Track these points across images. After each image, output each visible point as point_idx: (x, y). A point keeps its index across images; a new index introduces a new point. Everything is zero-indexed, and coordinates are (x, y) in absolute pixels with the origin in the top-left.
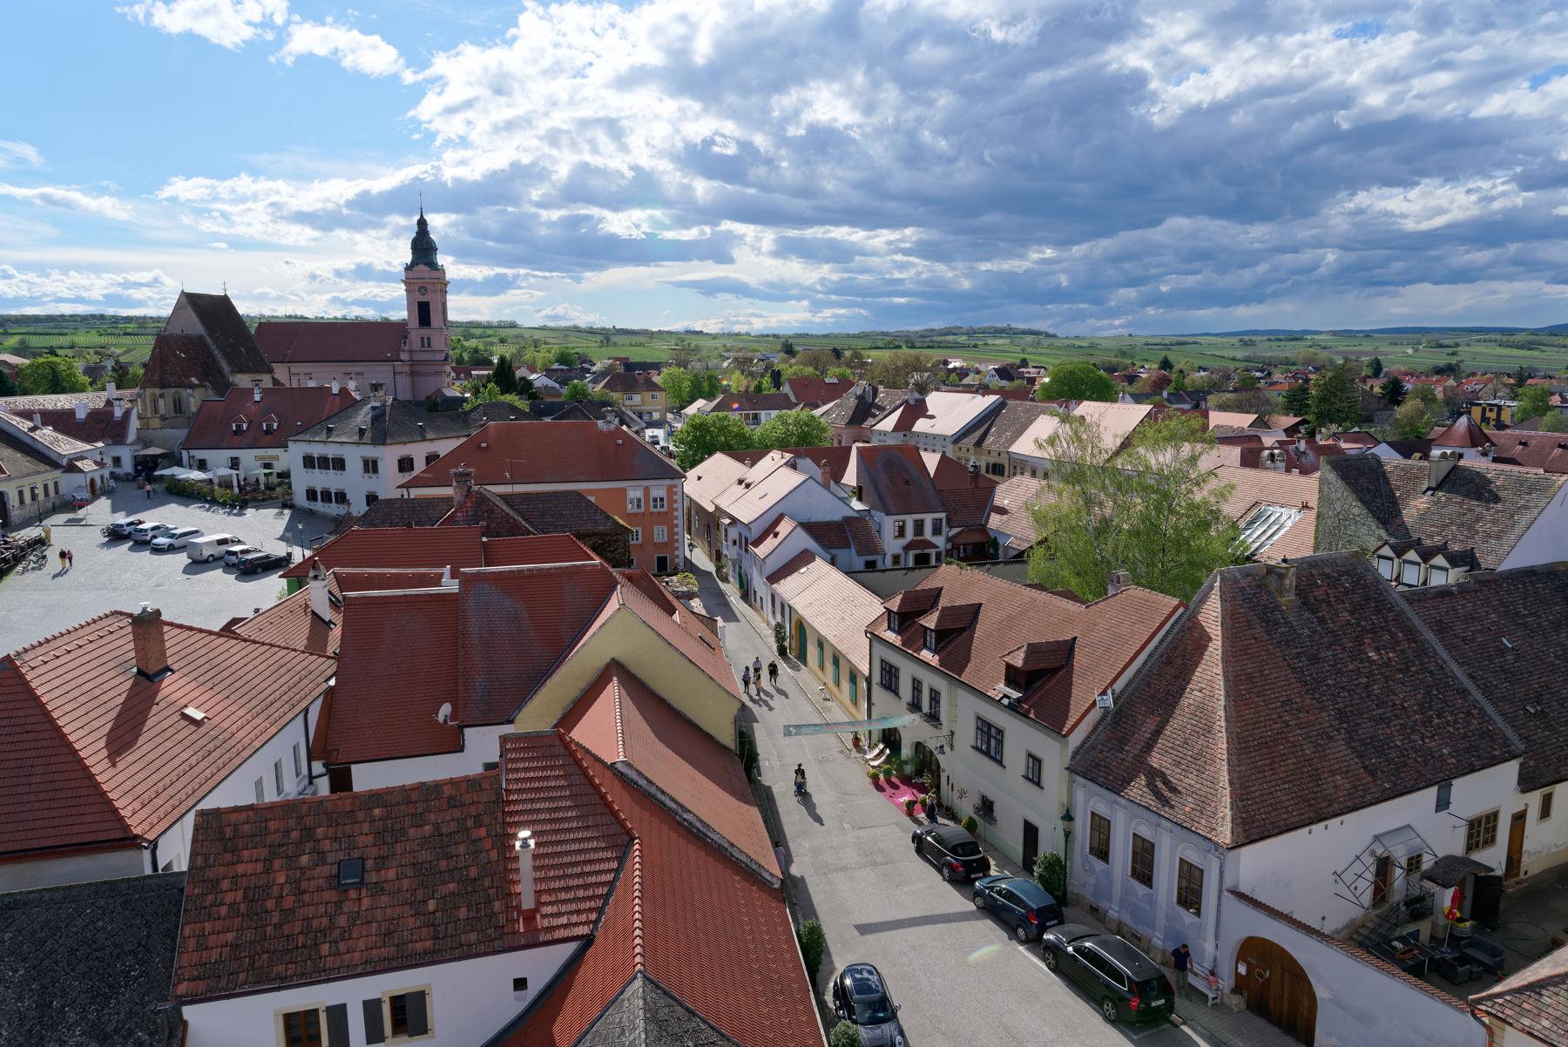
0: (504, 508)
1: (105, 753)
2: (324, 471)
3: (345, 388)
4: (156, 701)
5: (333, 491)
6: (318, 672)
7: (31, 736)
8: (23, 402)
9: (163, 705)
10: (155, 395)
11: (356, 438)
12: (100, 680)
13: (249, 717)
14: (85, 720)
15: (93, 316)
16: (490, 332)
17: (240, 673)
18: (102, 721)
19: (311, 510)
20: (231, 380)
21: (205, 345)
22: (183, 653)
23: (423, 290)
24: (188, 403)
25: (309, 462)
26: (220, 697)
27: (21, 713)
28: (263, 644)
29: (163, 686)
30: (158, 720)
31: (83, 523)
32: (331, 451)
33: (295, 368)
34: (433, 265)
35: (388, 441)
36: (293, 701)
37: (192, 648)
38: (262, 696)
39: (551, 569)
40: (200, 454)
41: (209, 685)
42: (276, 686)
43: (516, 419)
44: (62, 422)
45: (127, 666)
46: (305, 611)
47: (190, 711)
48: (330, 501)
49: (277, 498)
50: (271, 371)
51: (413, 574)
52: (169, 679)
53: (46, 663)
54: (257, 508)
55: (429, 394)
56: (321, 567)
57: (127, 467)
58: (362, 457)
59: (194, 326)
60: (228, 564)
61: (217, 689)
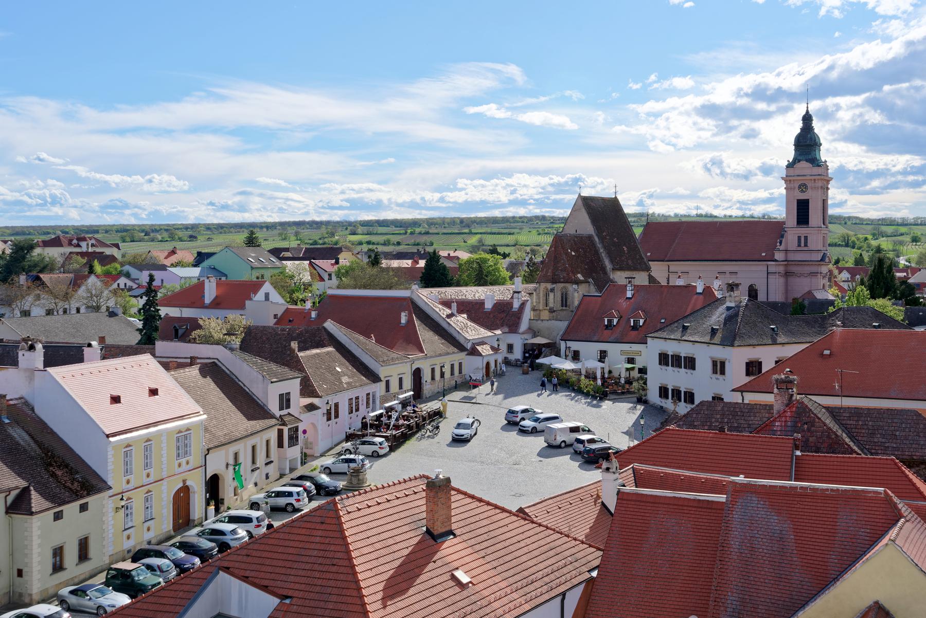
0: (828, 422)
1: (380, 595)
2: (676, 369)
3: (709, 287)
4: (433, 560)
5: (683, 390)
6: (584, 561)
7: (334, 569)
8: (450, 292)
9: (439, 563)
10: (547, 289)
11: (707, 339)
12: (395, 532)
13: (508, 590)
14: (375, 563)
15: (537, 217)
16: (903, 229)
17: (512, 548)
18: (387, 567)
19: (662, 407)
20: (611, 277)
21: (593, 244)
22: (468, 521)
23: (803, 187)
24: (573, 298)
25: (664, 359)
26: (489, 566)
27: (332, 548)
28: (540, 525)
29: (443, 547)
30: (431, 575)
31: (474, 401)
32: (684, 350)
33: (676, 266)
34: (815, 162)
35: (736, 343)
36: (553, 584)
37: (477, 518)
38: (526, 573)
39: (827, 490)
40: (575, 346)
41: (482, 553)
42: (541, 566)
43: (879, 327)
44: (473, 310)
45: (420, 524)
46: (595, 501)
47: (460, 574)
48: (667, 397)
49: (634, 393)
50: (648, 269)
51: (706, 479)
52: (450, 541)
53: (359, 510)
54: (614, 401)
55: (798, 295)
56: (614, 460)
57: (518, 354)
58: (711, 358)
59: (586, 227)
60: (576, 452)
61: (488, 559)
